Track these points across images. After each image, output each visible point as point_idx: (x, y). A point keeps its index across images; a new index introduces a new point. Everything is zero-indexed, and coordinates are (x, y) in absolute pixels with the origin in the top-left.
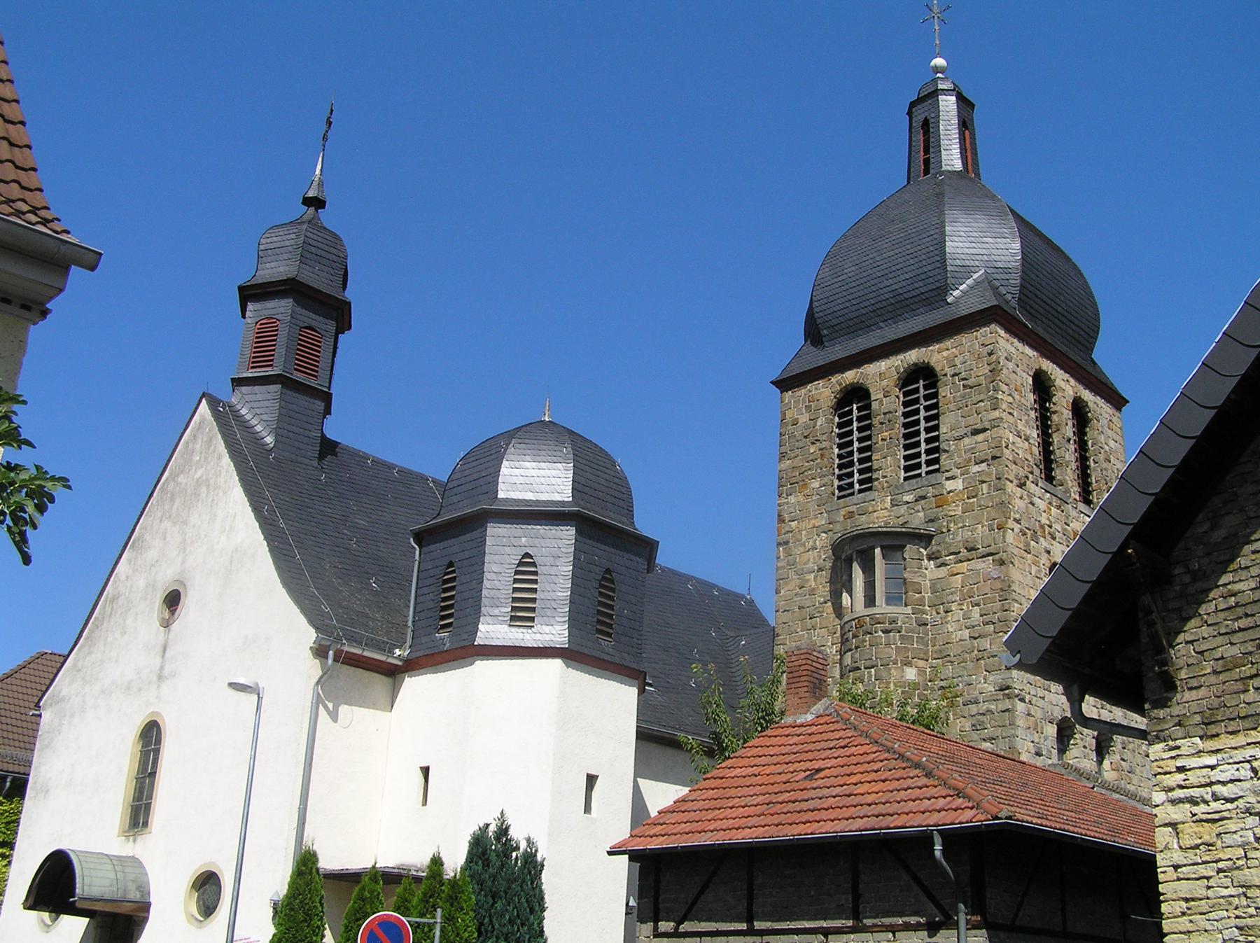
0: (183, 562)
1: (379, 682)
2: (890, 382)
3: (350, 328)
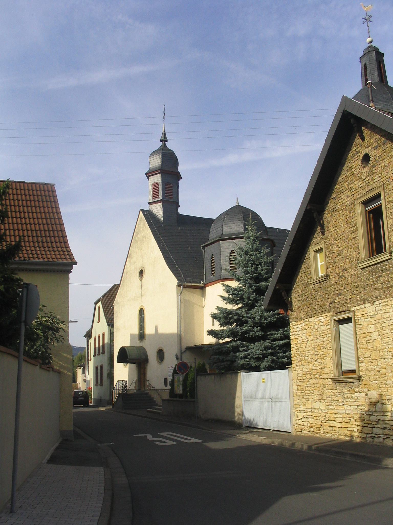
1: (198, 291)
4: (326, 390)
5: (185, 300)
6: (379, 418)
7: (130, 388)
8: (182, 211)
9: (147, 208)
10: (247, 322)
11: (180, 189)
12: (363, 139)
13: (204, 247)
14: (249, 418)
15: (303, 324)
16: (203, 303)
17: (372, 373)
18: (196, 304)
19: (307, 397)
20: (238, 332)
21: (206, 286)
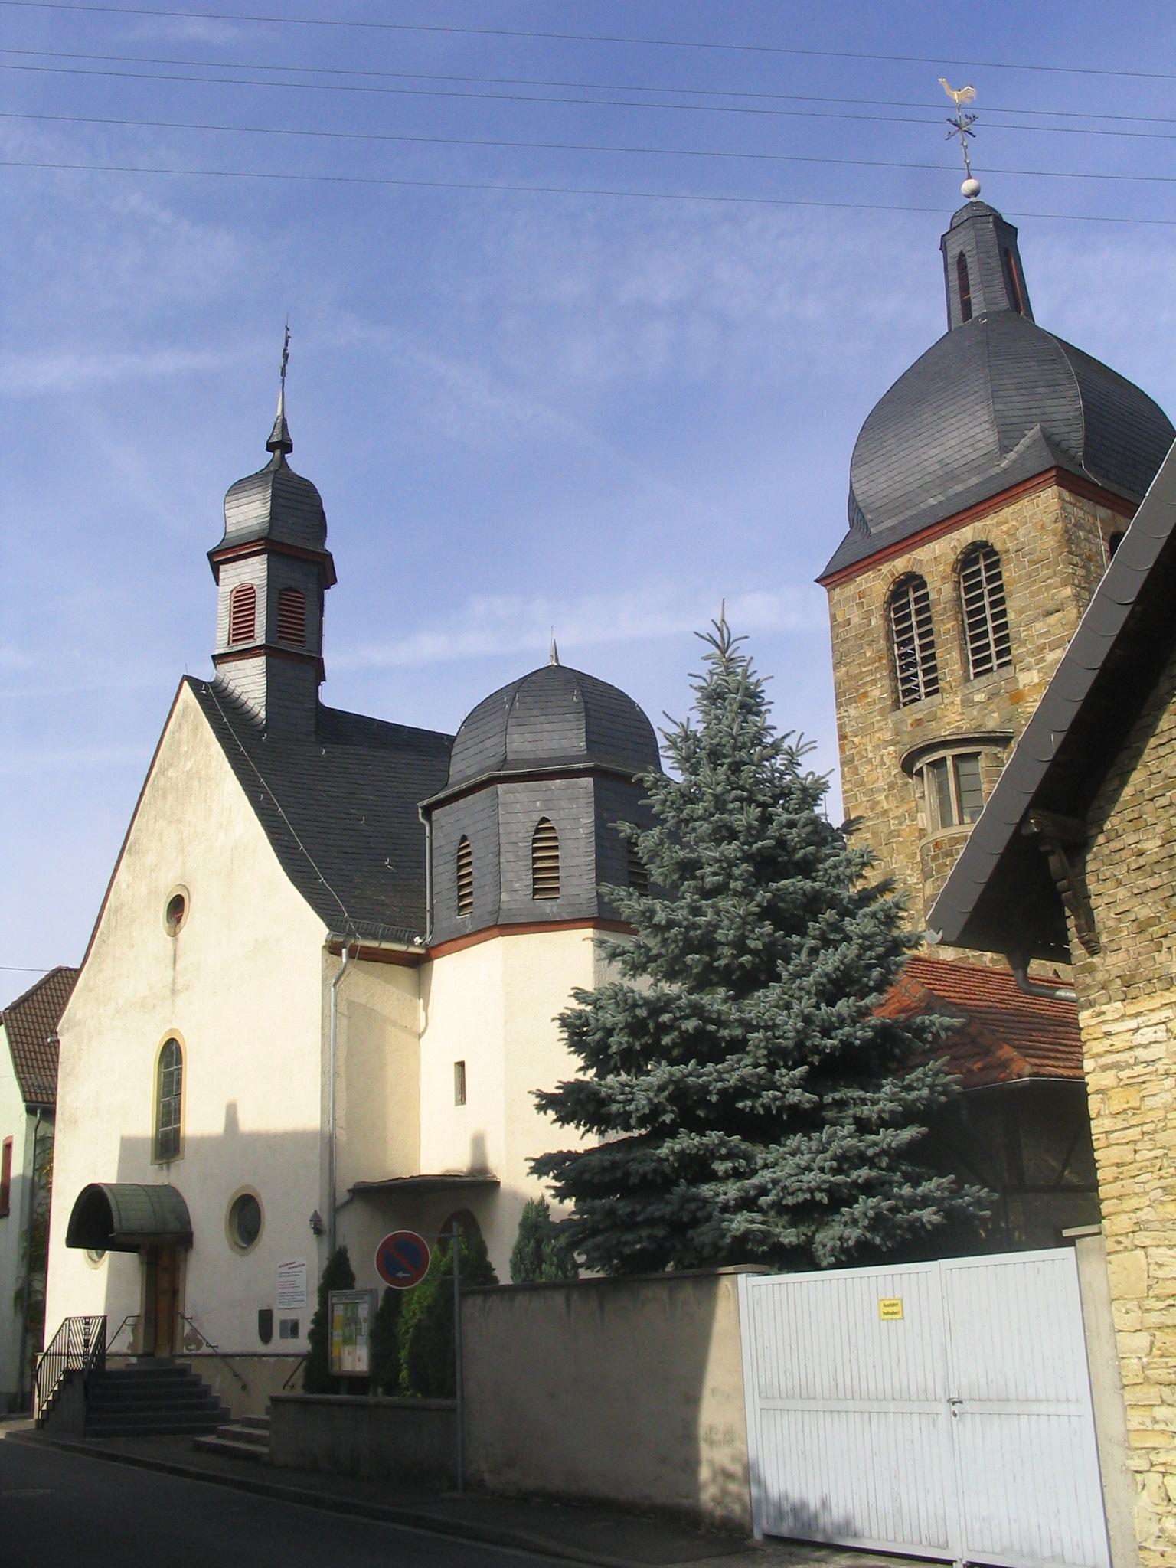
0: (184, 864)
2: (944, 568)
3: (335, 581)
5: (351, 1004)
7: (57, 1348)
8: (330, 696)
9: (207, 673)
10: (738, 1046)
11: (325, 619)
13: (428, 811)
14: (795, 1495)
16: (416, 1020)
18: (394, 1024)
20: (705, 1089)
21: (433, 953)
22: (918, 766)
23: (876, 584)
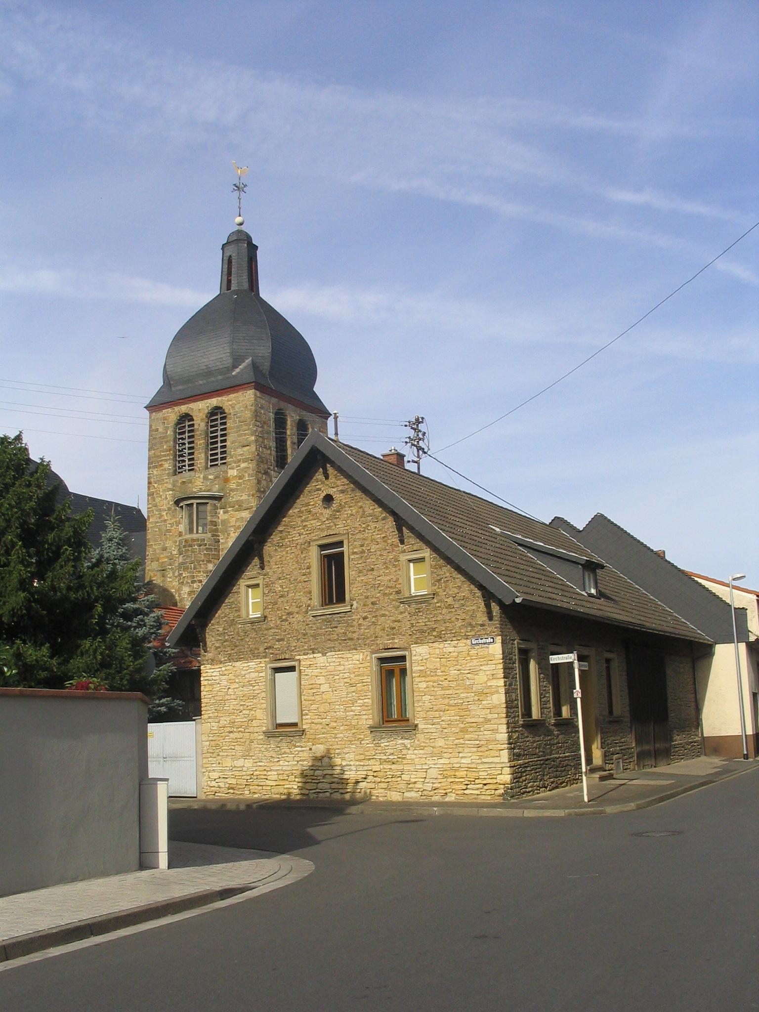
2: (202, 415)
4: (254, 745)
6: (325, 772)
12: (327, 477)
15: (223, 669)
17: (320, 727)
19: (225, 754)
22: (181, 504)
23: (171, 415)
